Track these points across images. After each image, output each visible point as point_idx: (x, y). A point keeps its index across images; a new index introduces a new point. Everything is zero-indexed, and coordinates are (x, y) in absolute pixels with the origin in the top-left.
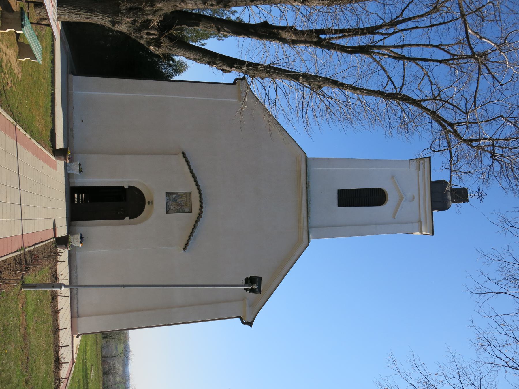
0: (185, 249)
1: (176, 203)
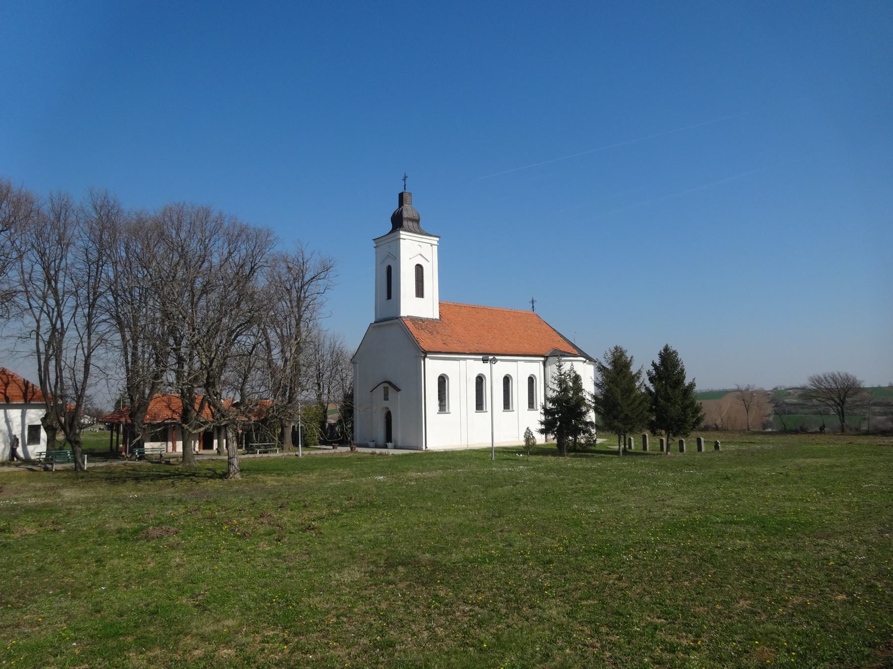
0: (399, 390)
1: (386, 399)
